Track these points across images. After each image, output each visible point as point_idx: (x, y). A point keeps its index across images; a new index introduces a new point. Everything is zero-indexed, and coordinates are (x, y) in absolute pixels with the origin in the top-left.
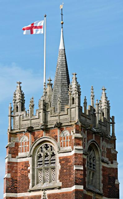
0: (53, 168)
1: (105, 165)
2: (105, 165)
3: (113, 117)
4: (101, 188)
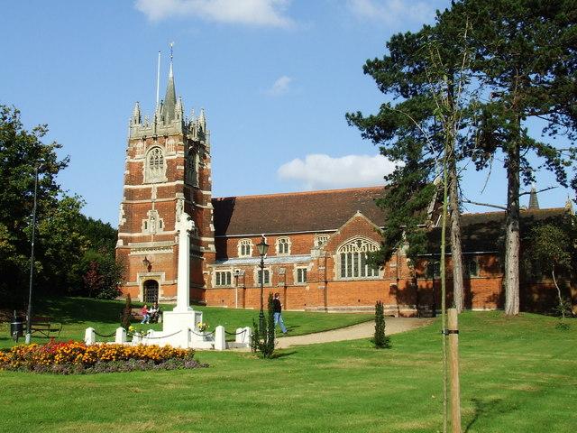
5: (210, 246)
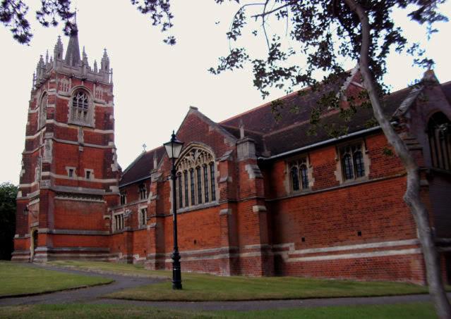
1: (98, 105)
5: (111, 188)
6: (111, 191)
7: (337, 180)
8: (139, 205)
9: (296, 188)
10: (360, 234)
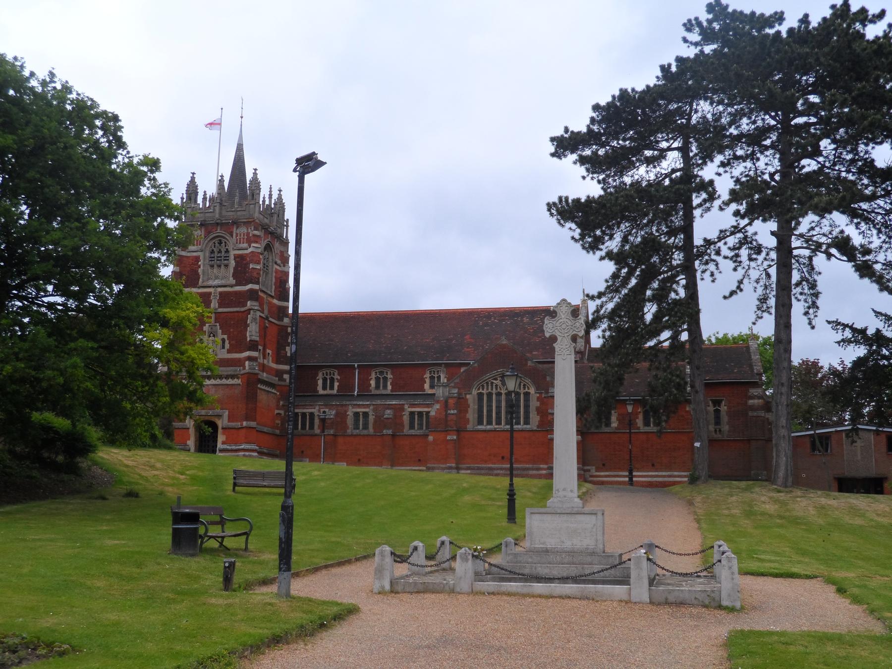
0: (226, 266)
2: (278, 268)
3: (288, 220)
4: (273, 290)
6: (285, 380)
7: (638, 426)
8: (350, 407)
9: (480, 422)
10: (653, 465)
